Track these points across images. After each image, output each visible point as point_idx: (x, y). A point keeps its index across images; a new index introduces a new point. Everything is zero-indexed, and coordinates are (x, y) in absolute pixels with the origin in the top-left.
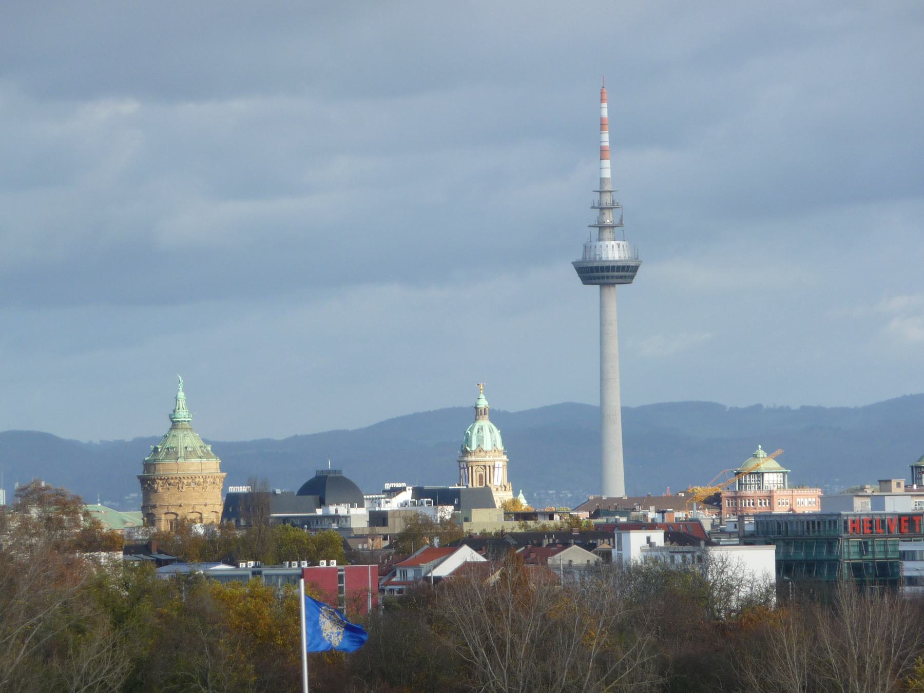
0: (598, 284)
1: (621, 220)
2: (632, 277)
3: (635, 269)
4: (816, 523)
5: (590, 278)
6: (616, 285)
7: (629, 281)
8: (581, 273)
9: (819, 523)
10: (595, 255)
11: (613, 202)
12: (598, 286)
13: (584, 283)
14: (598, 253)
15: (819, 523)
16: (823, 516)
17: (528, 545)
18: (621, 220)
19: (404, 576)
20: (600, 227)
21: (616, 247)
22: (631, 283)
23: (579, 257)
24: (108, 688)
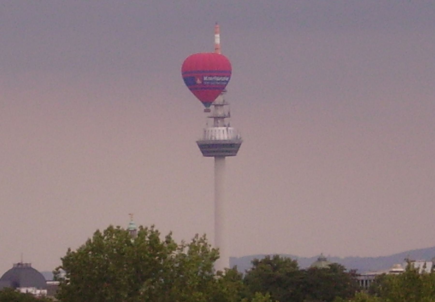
0: (212, 156)
1: (229, 113)
2: (236, 152)
3: (239, 146)
4: (364, 282)
5: (208, 152)
6: (226, 157)
7: (234, 154)
8: (202, 148)
9: (366, 281)
10: (212, 136)
11: (224, 101)
12: (213, 158)
13: (205, 155)
14: (213, 135)
15: (366, 281)
16: (370, 277)
17: (420, 278)
18: (229, 113)
19: (229, 152)
20: (215, 118)
21: (225, 131)
22: (235, 155)
23: (200, 137)
24: (200, 284)
